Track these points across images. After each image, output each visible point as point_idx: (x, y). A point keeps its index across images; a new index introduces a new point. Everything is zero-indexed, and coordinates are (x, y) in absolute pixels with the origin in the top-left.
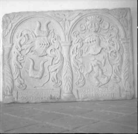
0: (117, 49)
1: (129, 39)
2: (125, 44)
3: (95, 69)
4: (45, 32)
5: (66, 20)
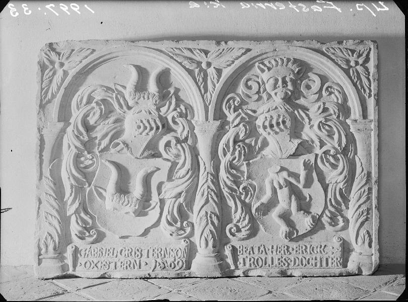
0: (340, 145)
1: (371, 121)
3: (283, 194)
5: (209, 64)
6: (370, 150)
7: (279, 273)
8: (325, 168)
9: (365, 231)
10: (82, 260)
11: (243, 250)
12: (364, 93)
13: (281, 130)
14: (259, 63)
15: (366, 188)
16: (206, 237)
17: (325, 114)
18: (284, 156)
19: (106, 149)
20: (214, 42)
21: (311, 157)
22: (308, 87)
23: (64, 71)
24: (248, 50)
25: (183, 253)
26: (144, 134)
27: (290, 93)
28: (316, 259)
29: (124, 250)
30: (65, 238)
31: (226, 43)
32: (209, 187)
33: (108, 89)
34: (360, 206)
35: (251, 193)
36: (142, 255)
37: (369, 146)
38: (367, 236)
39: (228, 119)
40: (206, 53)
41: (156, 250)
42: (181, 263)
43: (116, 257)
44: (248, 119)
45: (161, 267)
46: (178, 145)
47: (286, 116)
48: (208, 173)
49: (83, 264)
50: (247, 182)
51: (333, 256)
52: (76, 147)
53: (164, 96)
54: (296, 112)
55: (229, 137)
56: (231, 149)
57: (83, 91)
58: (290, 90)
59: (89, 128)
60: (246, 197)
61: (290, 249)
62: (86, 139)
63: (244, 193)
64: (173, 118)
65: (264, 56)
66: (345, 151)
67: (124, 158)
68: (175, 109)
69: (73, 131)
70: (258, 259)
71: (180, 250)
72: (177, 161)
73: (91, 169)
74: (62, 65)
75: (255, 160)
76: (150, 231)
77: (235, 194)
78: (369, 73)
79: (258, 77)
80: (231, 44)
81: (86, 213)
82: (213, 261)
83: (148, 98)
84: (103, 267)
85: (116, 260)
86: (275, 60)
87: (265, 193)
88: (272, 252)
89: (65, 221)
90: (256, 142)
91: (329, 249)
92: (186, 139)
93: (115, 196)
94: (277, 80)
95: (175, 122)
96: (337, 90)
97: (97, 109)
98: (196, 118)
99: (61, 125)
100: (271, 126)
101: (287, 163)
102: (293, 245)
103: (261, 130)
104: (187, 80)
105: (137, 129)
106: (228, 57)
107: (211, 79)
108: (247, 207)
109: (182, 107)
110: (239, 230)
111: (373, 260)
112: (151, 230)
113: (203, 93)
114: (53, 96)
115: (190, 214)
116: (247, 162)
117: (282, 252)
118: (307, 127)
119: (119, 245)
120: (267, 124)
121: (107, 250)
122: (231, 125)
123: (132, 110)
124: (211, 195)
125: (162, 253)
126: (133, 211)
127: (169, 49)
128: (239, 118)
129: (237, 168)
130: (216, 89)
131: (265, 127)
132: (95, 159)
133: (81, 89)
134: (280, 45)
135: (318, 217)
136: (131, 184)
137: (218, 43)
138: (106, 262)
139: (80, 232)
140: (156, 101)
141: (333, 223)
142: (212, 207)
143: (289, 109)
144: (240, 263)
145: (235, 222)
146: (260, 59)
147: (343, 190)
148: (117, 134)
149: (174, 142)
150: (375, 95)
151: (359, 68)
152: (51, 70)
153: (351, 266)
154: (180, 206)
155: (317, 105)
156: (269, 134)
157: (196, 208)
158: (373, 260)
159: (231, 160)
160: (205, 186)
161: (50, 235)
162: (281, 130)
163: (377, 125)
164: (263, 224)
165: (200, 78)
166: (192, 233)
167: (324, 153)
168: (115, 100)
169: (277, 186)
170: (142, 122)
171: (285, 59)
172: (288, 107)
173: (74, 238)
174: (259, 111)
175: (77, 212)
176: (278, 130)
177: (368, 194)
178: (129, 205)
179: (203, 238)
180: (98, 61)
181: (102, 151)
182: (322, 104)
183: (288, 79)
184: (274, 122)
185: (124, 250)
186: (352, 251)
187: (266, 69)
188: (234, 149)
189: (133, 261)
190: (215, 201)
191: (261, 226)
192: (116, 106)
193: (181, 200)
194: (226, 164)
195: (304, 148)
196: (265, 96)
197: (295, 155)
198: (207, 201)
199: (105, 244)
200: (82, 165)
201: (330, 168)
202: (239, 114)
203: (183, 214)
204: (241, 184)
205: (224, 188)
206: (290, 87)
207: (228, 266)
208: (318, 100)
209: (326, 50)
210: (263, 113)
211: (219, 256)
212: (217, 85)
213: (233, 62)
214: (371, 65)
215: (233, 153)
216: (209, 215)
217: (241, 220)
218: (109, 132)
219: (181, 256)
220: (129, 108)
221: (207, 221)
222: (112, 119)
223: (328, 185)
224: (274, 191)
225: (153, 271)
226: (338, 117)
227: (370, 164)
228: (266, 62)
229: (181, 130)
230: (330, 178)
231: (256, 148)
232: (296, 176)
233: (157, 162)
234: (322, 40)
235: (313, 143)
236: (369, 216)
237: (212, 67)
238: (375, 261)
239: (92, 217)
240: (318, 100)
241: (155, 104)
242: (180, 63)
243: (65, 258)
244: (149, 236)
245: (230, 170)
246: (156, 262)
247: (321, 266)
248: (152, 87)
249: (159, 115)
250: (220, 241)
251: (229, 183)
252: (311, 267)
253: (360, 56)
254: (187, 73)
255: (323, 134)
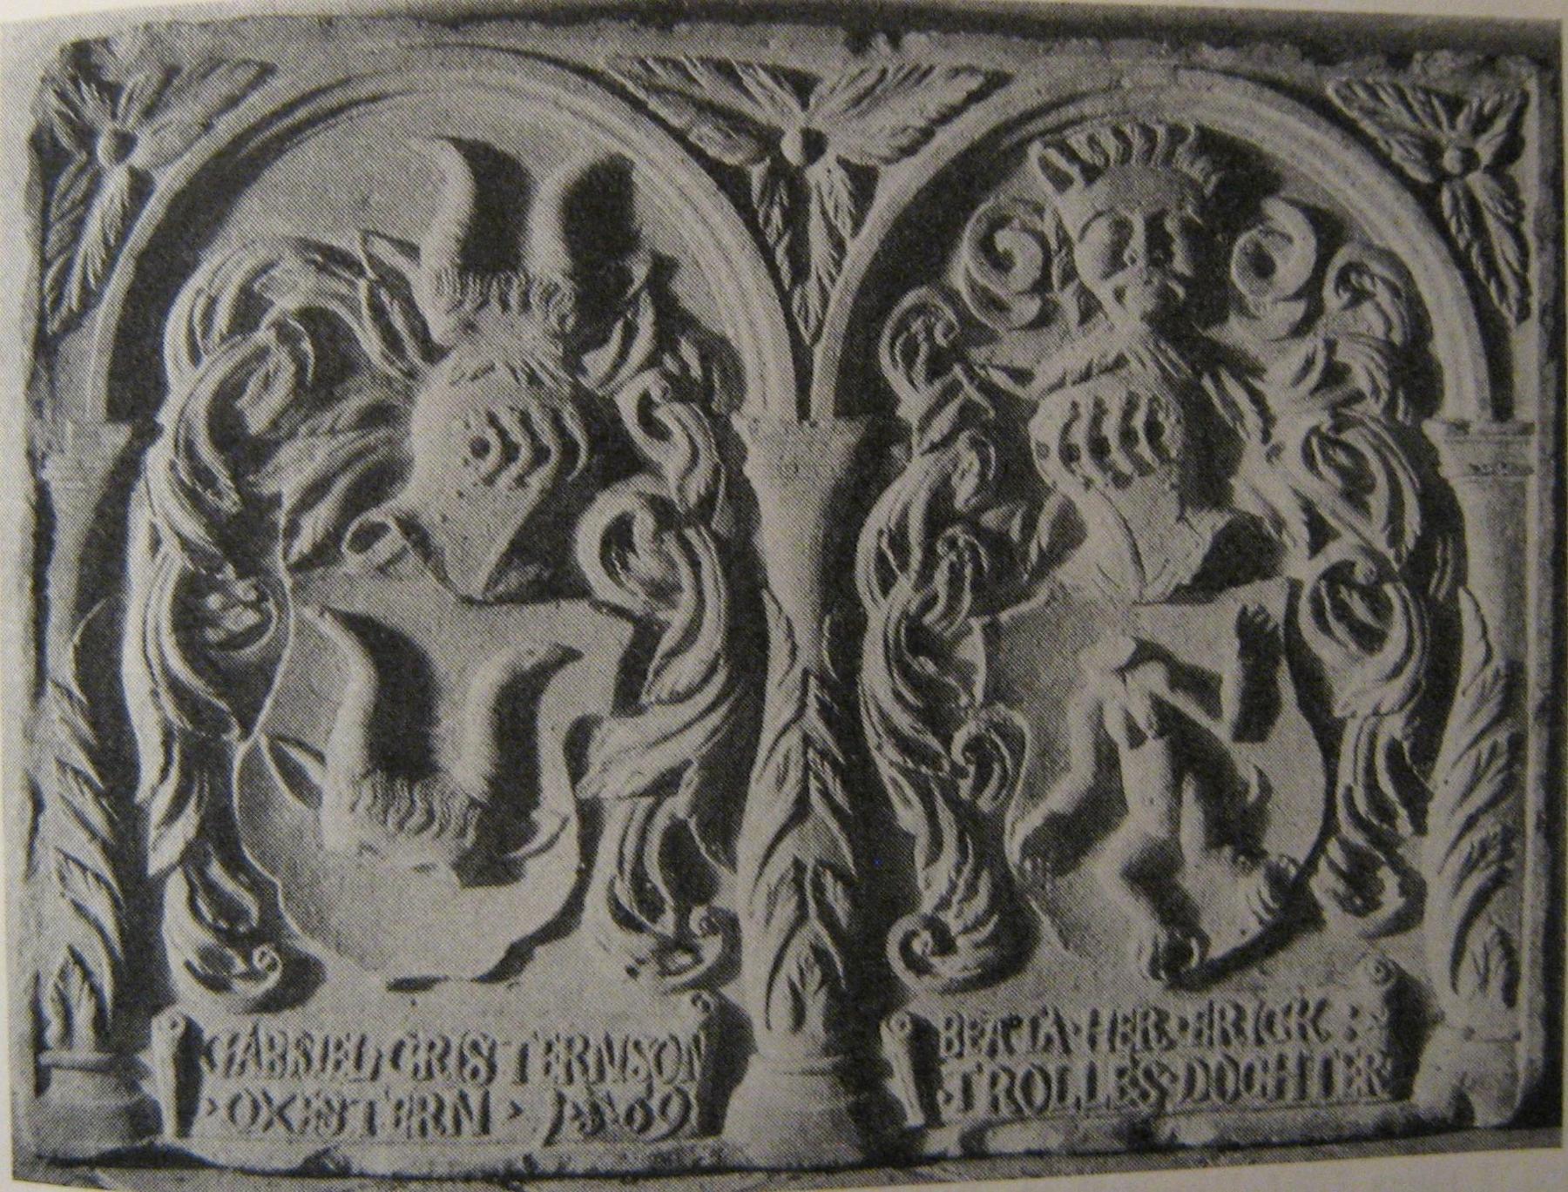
0: (1395, 537)
1: (1526, 429)
2: (716, 1153)
3: (1144, 771)
4: (549, 294)
5: (814, 145)
6: (1522, 563)
7: (1118, 1134)
8: (1329, 650)
9: (1493, 930)
10: (215, 1087)
11: (960, 1034)
12: (1501, 301)
13: (1143, 469)
14: (1046, 145)
15: (1501, 737)
16: (796, 978)
17: (1338, 394)
18: (1156, 589)
19: (324, 553)
20: (840, 34)
21: (1268, 597)
22: (1262, 266)
23: (133, 173)
24: (997, 81)
25: (685, 1058)
26: (505, 480)
27: (1180, 292)
28: (1281, 1064)
29: (410, 1043)
30: (139, 982)
31: (895, 41)
32: (807, 741)
33: (331, 260)
34: (1471, 823)
35: (1004, 770)
36: (492, 1068)
37: (1515, 548)
38: (1497, 954)
39: (901, 412)
40: (802, 85)
41: (560, 1048)
42: (675, 1108)
43: (375, 1074)
44: (992, 414)
45: (583, 1126)
46: (666, 536)
47: (1163, 401)
48: (806, 673)
49: (223, 1102)
50: (983, 714)
51: (1350, 1049)
52: (185, 544)
53: (599, 300)
54: (1207, 383)
55: (904, 498)
56: (916, 556)
57: (219, 271)
58: (1180, 278)
59: (245, 451)
60: (978, 789)
61: (1172, 1026)
62: (230, 503)
63: (972, 769)
64: (645, 405)
65: (1071, 112)
66: (1419, 569)
67: (411, 603)
68: (652, 361)
69: (173, 466)
70: (1028, 1078)
71: (671, 1047)
72: (661, 616)
73: (250, 653)
74: (125, 144)
75: (1024, 607)
76: (531, 958)
77: (930, 773)
78: (1520, 205)
79: (1039, 210)
80: (917, 44)
81: (235, 865)
82: (827, 1092)
83: (525, 305)
84: (313, 1122)
85: (372, 1091)
86: (1118, 133)
87: (1067, 768)
88: (1093, 1042)
89: (137, 899)
90: (1029, 526)
91: (1335, 1020)
92: (707, 502)
93: (367, 784)
94: (1122, 229)
95: (657, 431)
96: (1385, 281)
97: (281, 358)
98: (752, 403)
99: (118, 437)
100: (1099, 448)
101: (1164, 626)
102: (1187, 1007)
103: (1050, 468)
104: (716, 219)
105: (470, 456)
106: (909, 110)
107: (824, 213)
108: (981, 835)
109: (688, 352)
110: (945, 945)
111: (1521, 1064)
112: (540, 951)
113: (787, 282)
114: (89, 298)
115: (723, 871)
116: (987, 619)
117: (1138, 1039)
118: (1253, 449)
119: (390, 1023)
120: (1079, 436)
121: (331, 1047)
122: (915, 439)
123: (447, 365)
124: (818, 777)
125: (591, 1058)
126: (453, 858)
127: (626, 65)
128: (951, 410)
129: (941, 652)
130: (847, 263)
131: (1069, 455)
132: (271, 605)
133: (210, 262)
134: (1144, 71)
135: (1293, 871)
136: (440, 730)
137: (859, 44)
138: (328, 1103)
139: (206, 955)
140: (562, 320)
141: (1358, 902)
142: (825, 834)
143: (1178, 370)
144: (949, 1098)
145: (927, 906)
146: (1050, 119)
147: (1406, 745)
148: (380, 478)
149: (644, 525)
150: (1543, 312)
151: (1478, 182)
152: (82, 170)
153: (1429, 1093)
154: (676, 837)
155: (1300, 350)
156: (1088, 483)
157: (749, 845)
158: (1521, 1064)
159: (913, 608)
160: (793, 739)
161: (78, 960)
162: (1143, 469)
163: (1550, 448)
164: (1053, 913)
165: (768, 197)
166: (729, 966)
167: (1324, 576)
168: (365, 311)
169: (1117, 732)
170: (493, 420)
171: (1161, 131)
172: (1173, 355)
173: (182, 981)
174: (1046, 374)
175: (192, 858)
176: (1125, 466)
177: (1509, 765)
178: (435, 827)
179: (781, 990)
180: (288, 122)
181: (302, 566)
182: (1321, 345)
183: (1171, 225)
184: (1110, 428)
185: (410, 1043)
186: (1435, 1022)
187: (1074, 171)
188: (930, 561)
189: (450, 1098)
190: (836, 810)
191: (1045, 920)
192: (370, 343)
193: (679, 804)
194: (892, 627)
195: (1242, 554)
196: (1067, 300)
197: (1208, 583)
198: (801, 810)
199: (322, 1016)
200: (212, 635)
201: (1353, 647)
202: (952, 391)
203: (688, 867)
204: (959, 723)
205: (879, 748)
206: (1180, 264)
207: (892, 1109)
208: (1301, 329)
209: (1337, 91)
210: (1061, 384)
211: (856, 1069)
212: (852, 247)
213: (927, 134)
214: (1528, 169)
215: (925, 576)
216: (809, 875)
217: (955, 899)
218: (335, 475)
219: (682, 1079)
220: (433, 353)
221: (802, 905)
222: (352, 405)
223: (1342, 723)
224: (1107, 759)
225: (549, 1141)
226: (1391, 407)
227: (1519, 633)
228: (1077, 140)
229: (678, 463)
230: (1347, 693)
231: (1027, 553)
232: (1202, 685)
233: (568, 621)
234: (1321, 42)
235: (1279, 532)
236: (1510, 865)
237: (829, 159)
238: (1531, 1062)
239: (258, 887)
240: (1301, 329)
241: (556, 336)
242: (679, 136)
243: (145, 1073)
244: (531, 975)
245: (908, 658)
246: (561, 1099)
247: (1303, 1092)
248: (545, 248)
249: (576, 386)
250: (858, 994)
251: (903, 721)
252: (1258, 1103)
253: (1481, 124)
254: (708, 181)
255: (1325, 490)
